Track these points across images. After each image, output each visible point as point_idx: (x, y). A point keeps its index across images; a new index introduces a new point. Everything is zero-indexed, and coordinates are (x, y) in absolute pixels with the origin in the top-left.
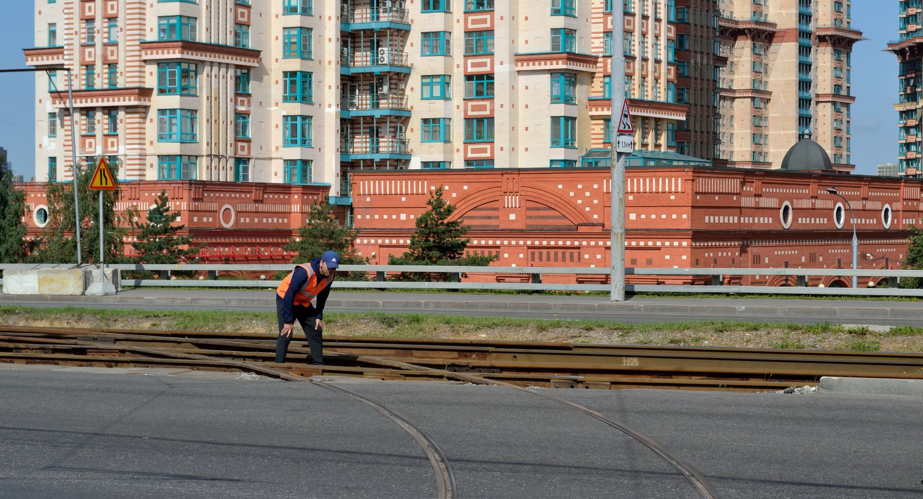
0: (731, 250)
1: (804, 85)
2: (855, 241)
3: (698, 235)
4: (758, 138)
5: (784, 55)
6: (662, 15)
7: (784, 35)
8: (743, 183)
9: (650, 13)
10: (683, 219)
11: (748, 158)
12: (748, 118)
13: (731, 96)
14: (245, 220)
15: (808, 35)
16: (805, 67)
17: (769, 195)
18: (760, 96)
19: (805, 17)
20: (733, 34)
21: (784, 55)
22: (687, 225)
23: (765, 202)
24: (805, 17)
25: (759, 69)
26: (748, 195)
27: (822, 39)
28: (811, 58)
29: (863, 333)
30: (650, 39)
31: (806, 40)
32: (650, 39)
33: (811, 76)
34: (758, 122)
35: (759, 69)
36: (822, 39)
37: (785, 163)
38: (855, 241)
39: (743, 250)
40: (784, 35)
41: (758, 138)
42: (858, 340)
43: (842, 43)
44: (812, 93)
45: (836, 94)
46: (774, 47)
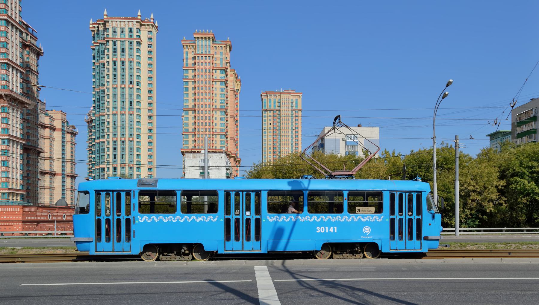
0: (34, 225)
1: (63, 186)
2: (55, 223)
3: (24, 222)
4: (51, 198)
5: (58, 180)
6: (19, 168)
7: (58, 174)
8: (37, 209)
9: (15, 167)
10: (20, 218)
11: (49, 203)
12: (49, 194)
13: (43, 188)
14: (68, 218)
15: (65, 175)
16: (63, 182)
17: (60, 213)
18: (52, 188)
19: (64, 170)
20: (44, 173)
21: (58, 180)
22: (21, 219)
23: (43, 214)
24: (64, 170)
25: (51, 182)
26: (39, 212)
27: (68, 176)
28: (65, 180)
29: (14, 249)
30: (15, 173)
31: (64, 176)
32: (15, 173)
33: (65, 184)
34: (51, 195)
35: (51, 182)
36: (68, 176)
37: (56, 204)
38: (55, 223)
39: (37, 225)
40: (58, 174)
41: (51, 198)
42: (12, 251)
43: (73, 177)
44: (65, 188)
45: (72, 189)
46: (55, 177)
